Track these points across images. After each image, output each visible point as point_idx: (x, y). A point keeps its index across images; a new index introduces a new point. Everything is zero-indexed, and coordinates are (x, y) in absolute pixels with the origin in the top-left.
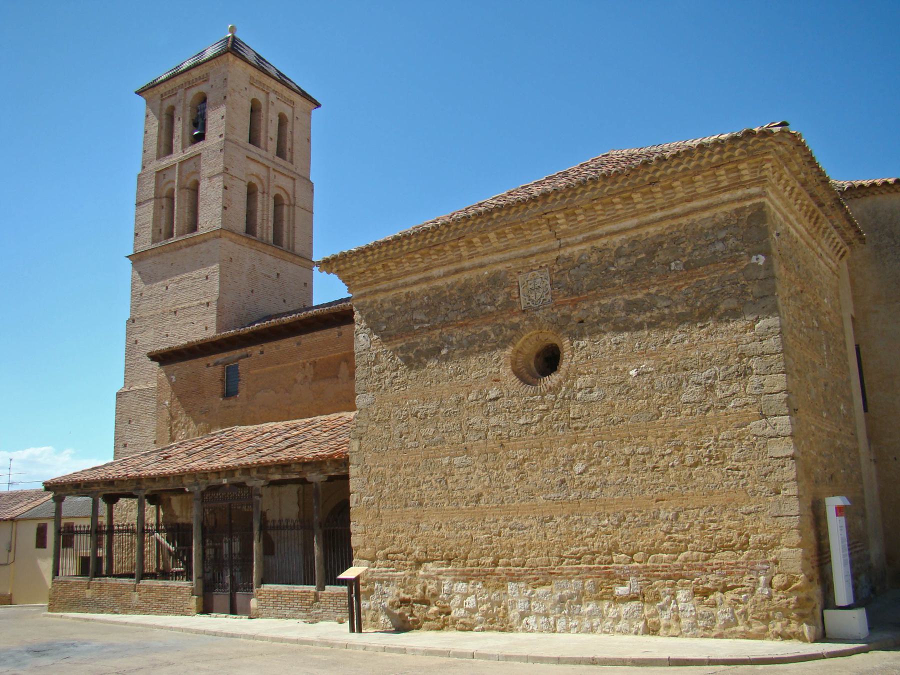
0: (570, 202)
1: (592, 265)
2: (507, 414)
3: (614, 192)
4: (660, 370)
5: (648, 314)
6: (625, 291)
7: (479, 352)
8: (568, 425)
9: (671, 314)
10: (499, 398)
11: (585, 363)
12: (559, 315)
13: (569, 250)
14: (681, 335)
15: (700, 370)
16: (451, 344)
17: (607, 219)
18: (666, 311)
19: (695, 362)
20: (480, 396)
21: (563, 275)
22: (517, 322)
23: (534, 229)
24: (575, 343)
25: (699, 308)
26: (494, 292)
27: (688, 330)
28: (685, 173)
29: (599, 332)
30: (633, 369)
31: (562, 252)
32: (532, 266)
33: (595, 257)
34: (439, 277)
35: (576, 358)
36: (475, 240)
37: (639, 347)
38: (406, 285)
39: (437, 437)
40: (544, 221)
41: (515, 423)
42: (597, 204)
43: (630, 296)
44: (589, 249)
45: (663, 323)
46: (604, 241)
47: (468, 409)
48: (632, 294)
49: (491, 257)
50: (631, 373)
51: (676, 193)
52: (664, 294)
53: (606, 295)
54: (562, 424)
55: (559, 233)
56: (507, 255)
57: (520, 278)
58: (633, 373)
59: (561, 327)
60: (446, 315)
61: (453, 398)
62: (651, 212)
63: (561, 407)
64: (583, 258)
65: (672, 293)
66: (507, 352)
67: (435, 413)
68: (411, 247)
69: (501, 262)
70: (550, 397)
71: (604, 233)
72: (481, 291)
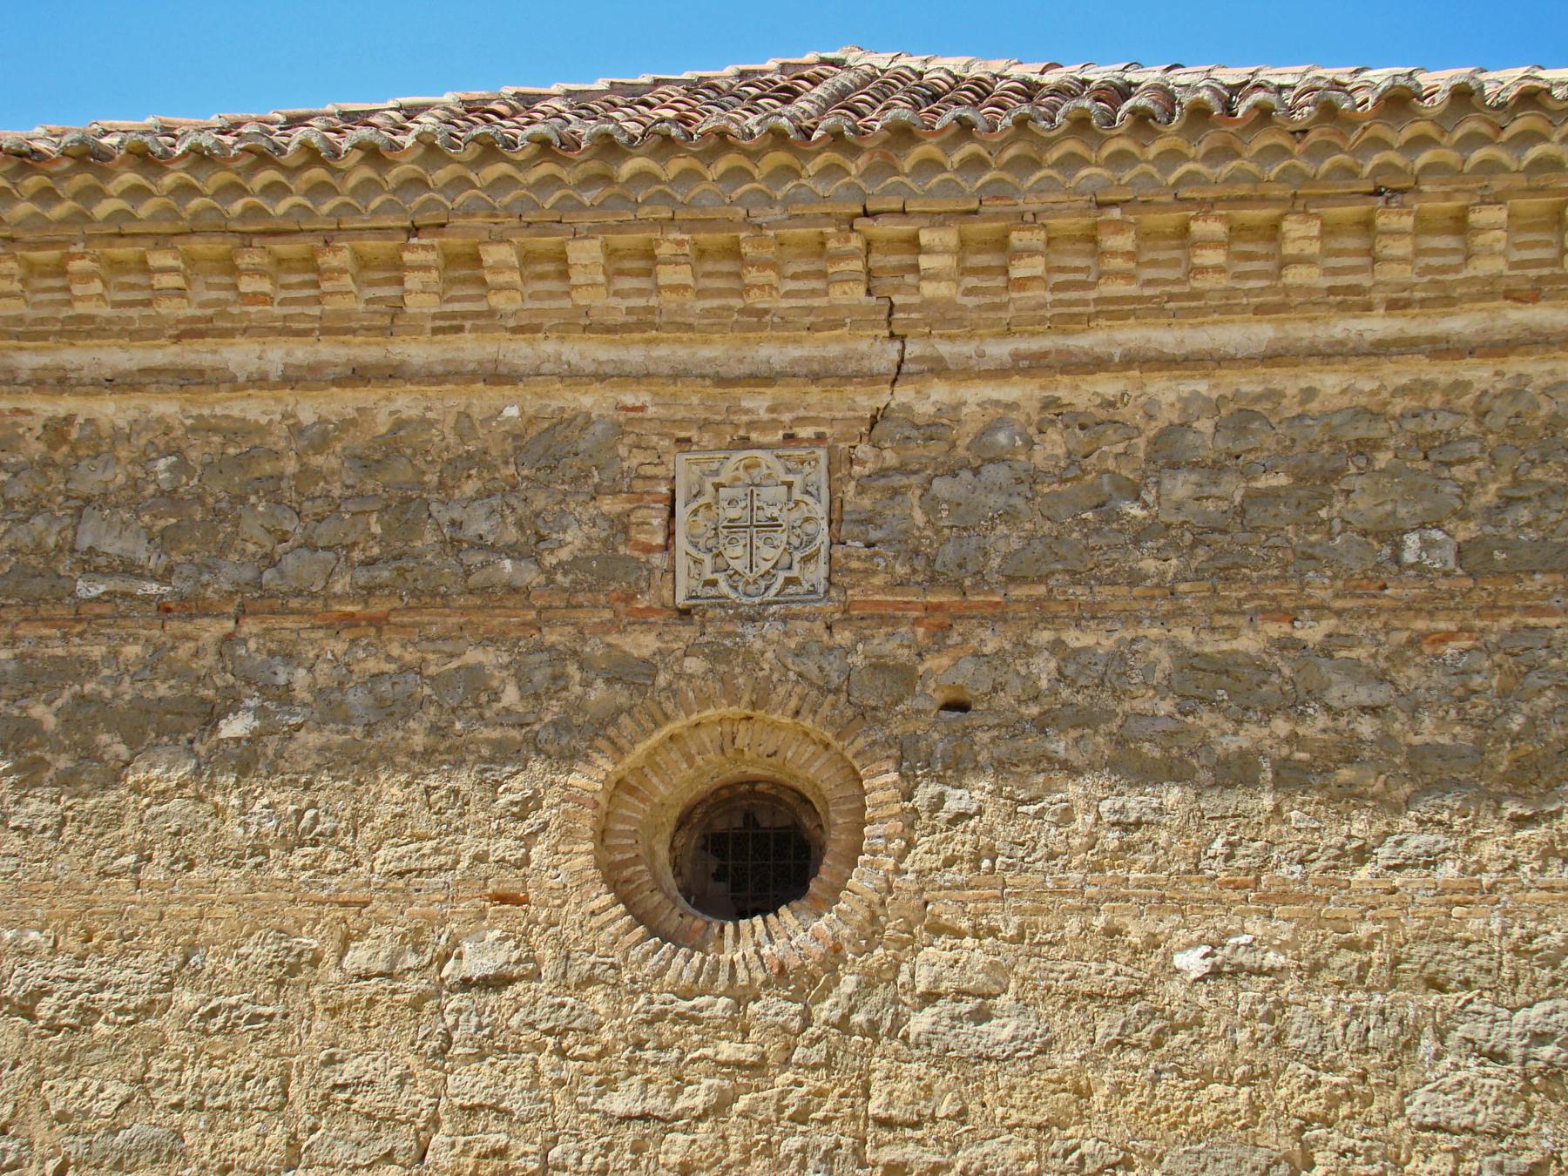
0: (998, 191)
1: (1034, 477)
2: (544, 1061)
3: (1209, 194)
4: (1316, 968)
5: (1281, 726)
6: (1181, 612)
7: (427, 755)
8: (857, 1151)
9: (1386, 739)
10: (511, 981)
11: (966, 885)
12: (857, 660)
13: (940, 392)
14: (1424, 838)
15: (1505, 998)
16: (285, 697)
17: (1139, 299)
18: (1366, 727)
19: (1482, 961)
20: (411, 960)
21: (895, 492)
22: (646, 653)
23: (791, 269)
24: (925, 793)
25: (1516, 738)
26: (540, 501)
27: (1458, 822)
28: (1540, 180)
29: (1047, 762)
30: (1189, 945)
31: (904, 394)
32: (752, 425)
33: (1054, 445)
34: (260, 381)
35: (919, 857)
36: (493, 254)
37: (1229, 857)
38: (62, 382)
39: (140, 1128)
40: (856, 242)
41: (581, 1109)
42: (1119, 227)
43: (1204, 635)
44: (1032, 407)
45: (1345, 774)
46: (1108, 385)
47: (333, 1012)
48: (1213, 629)
49: (549, 347)
50: (1179, 960)
51: (1468, 256)
52: (1359, 653)
53: (1093, 614)
54: (826, 1142)
55: (906, 308)
56: (634, 355)
57: (685, 469)
58: (1192, 962)
59: (863, 714)
60: (271, 561)
61: (259, 951)
62: (1343, 307)
63: (828, 1064)
64: (1002, 438)
65: (1397, 657)
66: (576, 779)
67: (146, 1010)
68: (144, 210)
69: (600, 378)
70: (774, 1008)
71: (1117, 353)
72: (470, 488)
